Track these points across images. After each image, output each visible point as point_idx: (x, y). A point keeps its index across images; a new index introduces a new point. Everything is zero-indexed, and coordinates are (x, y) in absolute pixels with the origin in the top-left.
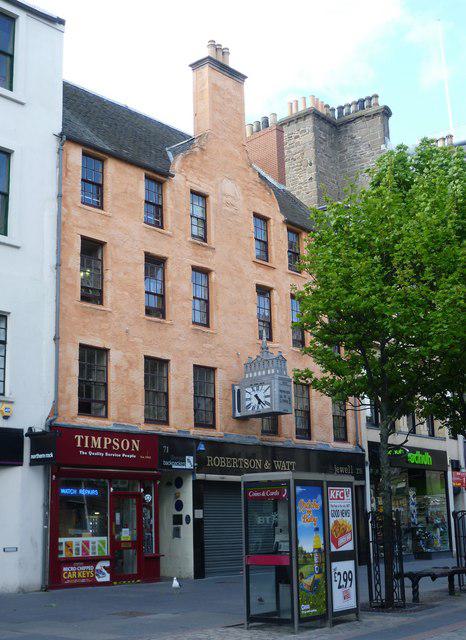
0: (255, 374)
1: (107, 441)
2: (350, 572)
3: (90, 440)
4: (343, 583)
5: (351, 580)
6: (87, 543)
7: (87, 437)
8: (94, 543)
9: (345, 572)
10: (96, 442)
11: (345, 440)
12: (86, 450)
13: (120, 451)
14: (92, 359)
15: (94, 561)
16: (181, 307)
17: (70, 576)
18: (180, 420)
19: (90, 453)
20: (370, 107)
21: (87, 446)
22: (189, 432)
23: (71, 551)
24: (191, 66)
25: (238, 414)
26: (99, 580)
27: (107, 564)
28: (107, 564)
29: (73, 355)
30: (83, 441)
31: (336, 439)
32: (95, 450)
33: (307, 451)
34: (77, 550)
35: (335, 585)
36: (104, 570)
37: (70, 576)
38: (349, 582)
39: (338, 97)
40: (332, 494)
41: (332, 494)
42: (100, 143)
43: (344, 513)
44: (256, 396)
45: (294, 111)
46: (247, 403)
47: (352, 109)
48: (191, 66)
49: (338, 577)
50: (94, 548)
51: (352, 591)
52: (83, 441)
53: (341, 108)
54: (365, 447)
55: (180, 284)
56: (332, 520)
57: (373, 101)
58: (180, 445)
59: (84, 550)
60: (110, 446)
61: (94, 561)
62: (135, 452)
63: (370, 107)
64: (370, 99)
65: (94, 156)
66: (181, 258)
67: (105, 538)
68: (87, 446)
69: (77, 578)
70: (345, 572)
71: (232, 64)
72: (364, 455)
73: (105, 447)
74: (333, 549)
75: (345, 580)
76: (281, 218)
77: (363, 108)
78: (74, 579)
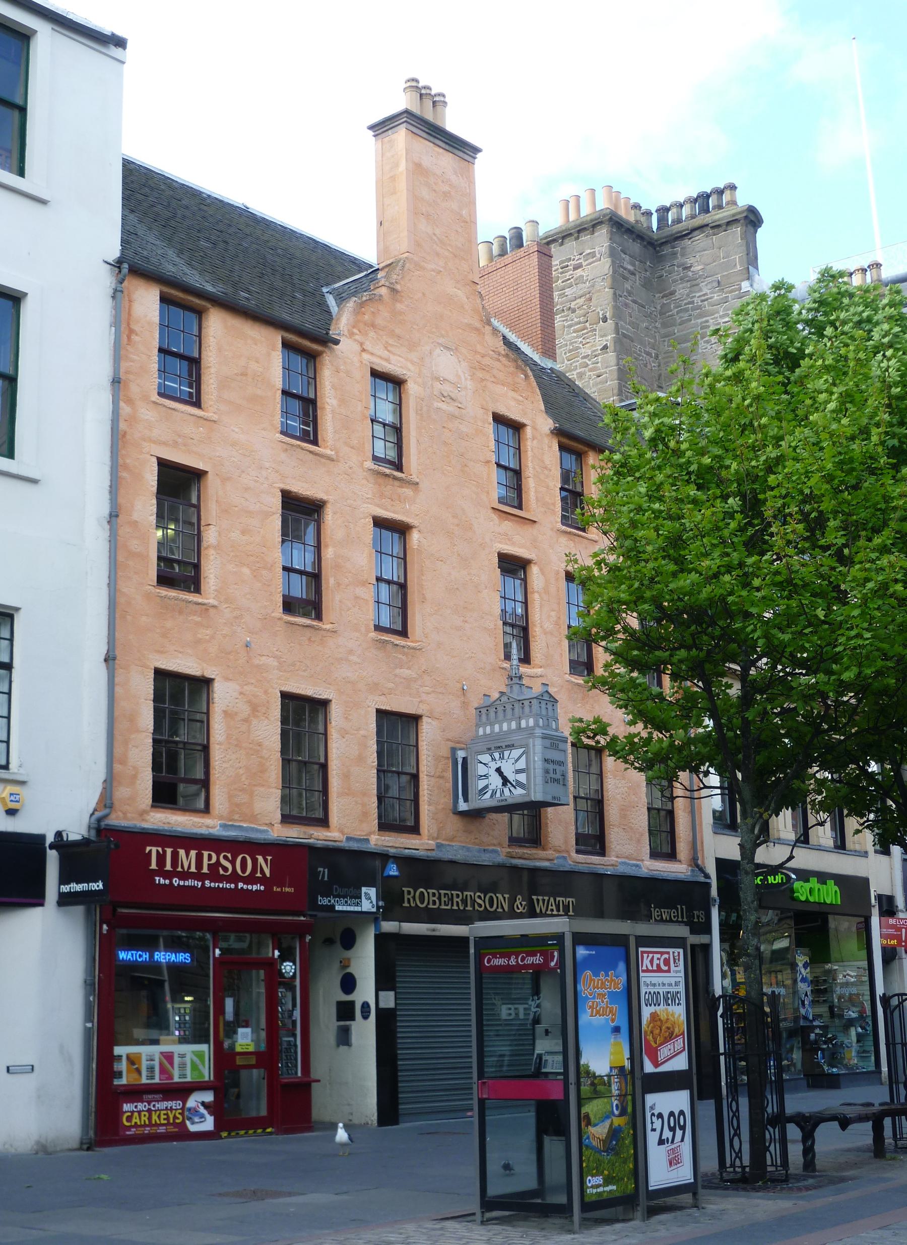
0: (497, 728)
2: (682, 1113)
3: (175, 856)
4: (667, 1134)
5: (683, 1128)
6: (169, 1057)
7: (169, 851)
8: (182, 1056)
9: (672, 1114)
10: (188, 860)
11: (672, 855)
13: (234, 878)
15: (183, 1091)
17: (136, 1119)
19: (176, 882)
20: (720, 207)
21: (168, 867)
23: (138, 1071)
25: (463, 806)
26: (192, 1128)
27: (208, 1097)
28: (209, 1097)
30: (161, 858)
32: (185, 875)
33: (598, 877)
34: (151, 1069)
35: (652, 1138)
36: (202, 1110)
37: (136, 1119)
38: (679, 1133)
39: (658, 188)
43: (671, 999)
45: (572, 217)
46: (482, 784)
47: (686, 211)
49: (658, 1124)
52: (161, 858)
53: (663, 211)
57: (726, 197)
59: (163, 1070)
60: (214, 867)
61: (183, 1091)
62: (263, 880)
63: (720, 207)
64: (720, 192)
65: (185, 303)
67: (204, 1047)
68: (168, 867)
69: (150, 1125)
70: (672, 1114)
71: (453, 124)
72: (708, 885)
73: (205, 870)
74: (649, 1068)
77: (705, 210)
78: (145, 1126)
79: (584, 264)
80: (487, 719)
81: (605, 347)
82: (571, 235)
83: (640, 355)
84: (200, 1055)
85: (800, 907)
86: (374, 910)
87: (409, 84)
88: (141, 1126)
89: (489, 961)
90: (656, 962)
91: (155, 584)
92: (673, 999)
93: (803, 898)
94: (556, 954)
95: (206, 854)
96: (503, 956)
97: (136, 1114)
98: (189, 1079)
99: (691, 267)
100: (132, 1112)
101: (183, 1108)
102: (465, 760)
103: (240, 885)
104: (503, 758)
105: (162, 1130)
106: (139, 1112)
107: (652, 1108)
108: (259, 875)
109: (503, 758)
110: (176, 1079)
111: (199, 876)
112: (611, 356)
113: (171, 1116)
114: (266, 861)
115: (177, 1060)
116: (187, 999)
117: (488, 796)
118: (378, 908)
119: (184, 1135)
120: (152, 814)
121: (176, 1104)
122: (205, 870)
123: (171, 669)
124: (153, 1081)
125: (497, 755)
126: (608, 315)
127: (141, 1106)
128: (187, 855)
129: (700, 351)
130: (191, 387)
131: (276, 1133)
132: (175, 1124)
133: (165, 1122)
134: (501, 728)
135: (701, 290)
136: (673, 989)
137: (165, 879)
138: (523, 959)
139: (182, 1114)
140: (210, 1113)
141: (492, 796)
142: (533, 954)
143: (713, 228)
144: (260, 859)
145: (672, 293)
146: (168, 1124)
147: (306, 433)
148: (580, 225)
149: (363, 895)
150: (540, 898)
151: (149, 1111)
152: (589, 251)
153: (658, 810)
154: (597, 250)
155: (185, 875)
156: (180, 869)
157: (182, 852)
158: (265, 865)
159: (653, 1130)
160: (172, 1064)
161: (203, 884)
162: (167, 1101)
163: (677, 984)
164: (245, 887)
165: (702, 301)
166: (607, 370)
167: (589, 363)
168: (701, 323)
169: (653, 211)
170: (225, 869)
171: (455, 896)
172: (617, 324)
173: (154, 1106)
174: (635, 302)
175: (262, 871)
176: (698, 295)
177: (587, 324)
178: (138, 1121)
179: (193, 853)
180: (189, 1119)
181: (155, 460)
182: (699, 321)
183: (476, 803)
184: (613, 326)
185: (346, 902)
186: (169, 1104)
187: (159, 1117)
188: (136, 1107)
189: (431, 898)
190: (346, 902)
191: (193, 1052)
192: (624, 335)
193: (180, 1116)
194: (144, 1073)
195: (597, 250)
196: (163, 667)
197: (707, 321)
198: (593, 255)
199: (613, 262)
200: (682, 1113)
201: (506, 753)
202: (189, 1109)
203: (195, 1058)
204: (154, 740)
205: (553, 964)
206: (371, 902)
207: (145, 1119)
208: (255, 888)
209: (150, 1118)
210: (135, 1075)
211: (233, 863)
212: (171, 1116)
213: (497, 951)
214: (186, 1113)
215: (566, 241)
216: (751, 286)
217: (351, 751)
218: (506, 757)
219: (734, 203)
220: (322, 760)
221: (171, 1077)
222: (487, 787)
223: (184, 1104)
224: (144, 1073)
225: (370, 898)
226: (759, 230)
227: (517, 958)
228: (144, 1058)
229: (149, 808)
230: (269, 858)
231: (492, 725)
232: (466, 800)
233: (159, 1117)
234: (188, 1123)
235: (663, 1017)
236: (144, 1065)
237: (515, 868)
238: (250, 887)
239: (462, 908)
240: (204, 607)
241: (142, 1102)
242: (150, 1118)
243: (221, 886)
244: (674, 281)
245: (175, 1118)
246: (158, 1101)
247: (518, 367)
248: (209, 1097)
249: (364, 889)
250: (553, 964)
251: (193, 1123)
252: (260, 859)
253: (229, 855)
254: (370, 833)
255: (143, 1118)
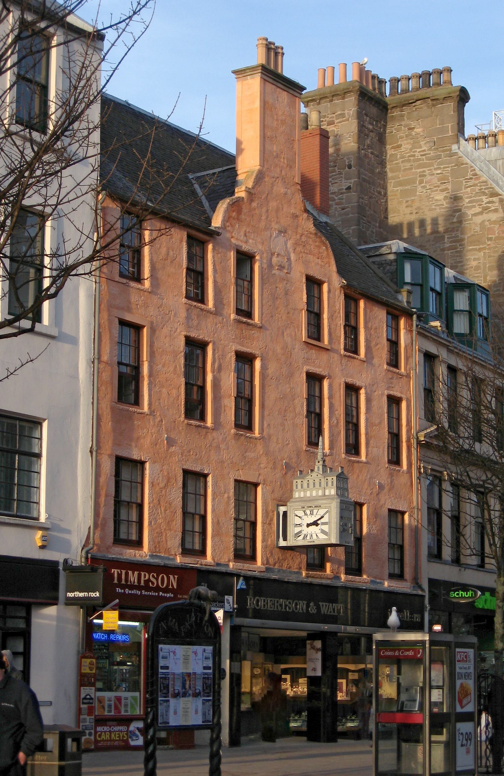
0: (308, 494)
1: (145, 576)
2: (470, 733)
3: (127, 574)
4: (465, 742)
5: (470, 740)
6: (119, 699)
7: (124, 572)
8: (126, 699)
9: (467, 733)
10: (133, 577)
11: (400, 576)
12: (123, 587)
13: (157, 589)
14: (125, 470)
15: (127, 721)
16: (221, 405)
17: (103, 737)
18: (217, 552)
19: (127, 591)
20: (439, 84)
21: (123, 582)
22: (228, 565)
23: (103, 707)
24: (234, 72)
25: (282, 543)
26: (132, 743)
27: (141, 724)
28: (141, 725)
29: (108, 466)
30: (120, 575)
31: (392, 576)
32: (132, 587)
33: (356, 591)
34: (110, 706)
35: (458, 743)
36: (137, 732)
37: (103, 737)
38: (469, 742)
39: (393, 64)
40: (459, 656)
41: (459, 656)
42: (141, 198)
43: (467, 676)
44: (308, 525)
45: (328, 83)
46: (297, 530)
47: (412, 84)
48: (234, 72)
49: (461, 737)
50: (126, 705)
51: (472, 748)
52: (120, 575)
53: (395, 81)
54: (425, 585)
55: (220, 378)
56: (458, 683)
57: (444, 77)
58: (218, 580)
59: (116, 708)
60: (147, 581)
61: (127, 721)
62: (172, 591)
63: (439, 84)
64: (440, 73)
65: (135, 215)
66: (223, 342)
67: (137, 694)
68: (123, 582)
69: (111, 740)
70: (467, 733)
71: (288, 72)
72: (423, 597)
73: (142, 583)
74: (459, 709)
75: (467, 740)
76: (337, 281)
77: (427, 85)
78: (108, 741)
79: (336, 121)
80: (302, 487)
81: (349, 188)
82: (326, 97)
83: (374, 194)
84: (134, 698)
85: (479, 613)
86: (231, 610)
87: (261, 42)
88: (105, 741)
89: (383, 653)
90: (462, 656)
91: (117, 401)
92: (468, 676)
93: (481, 607)
94: (421, 651)
95: (143, 573)
96: (391, 650)
97: (103, 733)
98: (129, 713)
99: (414, 128)
100: (102, 732)
101: (127, 731)
102: (285, 513)
103: (161, 593)
104: (313, 514)
105: (116, 743)
106: (105, 732)
107: (459, 730)
108: (170, 587)
109: (313, 514)
110: (123, 713)
111: (139, 588)
112: (353, 195)
113: (121, 736)
114: (174, 578)
115: (123, 701)
116: (128, 664)
117: (301, 538)
118: (234, 609)
119: (127, 747)
120: (113, 548)
121: (123, 728)
122: (142, 583)
123: (124, 456)
124: (111, 714)
125: (308, 512)
126: (352, 163)
127: (106, 728)
128: (133, 574)
129: (418, 193)
130: (133, 268)
131: (176, 749)
132: (123, 741)
133: (118, 739)
134: (311, 494)
135: (421, 147)
136: (469, 671)
137: (121, 589)
138: (402, 653)
139: (127, 734)
140: (142, 735)
141: (304, 538)
142: (408, 650)
143: (432, 100)
144: (171, 577)
145: (399, 146)
146: (120, 740)
147: (197, 294)
148: (334, 92)
149: (226, 600)
150: (324, 604)
151: (110, 732)
152: (339, 113)
153: (394, 545)
154: (346, 112)
155: (132, 587)
156: (129, 583)
157: (130, 573)
158: (174, 581)
159: (459, 740)
160: (120, 703)
161: (141, 593)
162: (119, 726)
163: (195, 653)
164: (163, 594)
165: (422, 155)
166: (350, 205)
167: (336, 198)
168: (420, 172)
169: (387, 80)
170: (153, 583)
171: (276, 602)
172: (359, 171)
173: (113, 729)
174: (372, 153)
175: (172, 585)
176: (418, 150)
177: (336, 168)
178: (104, 737)
179: (136, 573)
180: (131, 737)
181: (117, 320)
182: (419, 170)
183: (291, 542)
184: (356, 173)
185: (216, 605)
186: (120, 728)
187: (115, 735)
188: (103, 729)
189: (265, 603)
190: (216, 605)
191: (131, 697)
192: (364, 180)
193: (126, 736)
194: (106, 709)
195: (346, 112)
196: (120, 454)
197: (424, 171)
198: (343, 115)
199: (359, 123)
200: (470, 733)
201: (315, 511)
202: (131, 732)
203: (133, 701)
204: (115, 501)
205: (419, 656)
206: (230, 605)
207: (108, 736)
208: (168, 595)
209: (110, 736)
210: (102, 710)
211: (157, 579)
212: (121, 736)
213: (387, 648)
214: (129, 734)
215: (322, 101)
216: (459, 148)
217: (218, 505)
218: (315, 513)
219: (450, 83)
220: (202, 512)
221: (120, 712)
222: (300, 532)
223: (128, 727)
224: (106, 709)
225: (229, 603)
226: (467, 104)
227: (399, 652)
228: (106, 699)
229: (112, 544)
230: (176, 577)
231: (305, 491)
232: (285, 539)
233: (115, 735)
234: (130, 740)
235: (464, 685)
236: (106, 703)
237: (311, 585)
238: (166, 595)
239: (280, 610)
240: (143, 415)
241: (107, 726)
242: (110, 736)
243: (150, 594)
244: (401, 138)
245: (123, 737)
246: (114, 726)
247: (322, 242)
248: (141, 725)
249: (226, 597)
250: (419, 656)
251: (133, 740)
252: (171, 577)
253: (155, 575)
254: (229, 561)
255: (107, 736)
